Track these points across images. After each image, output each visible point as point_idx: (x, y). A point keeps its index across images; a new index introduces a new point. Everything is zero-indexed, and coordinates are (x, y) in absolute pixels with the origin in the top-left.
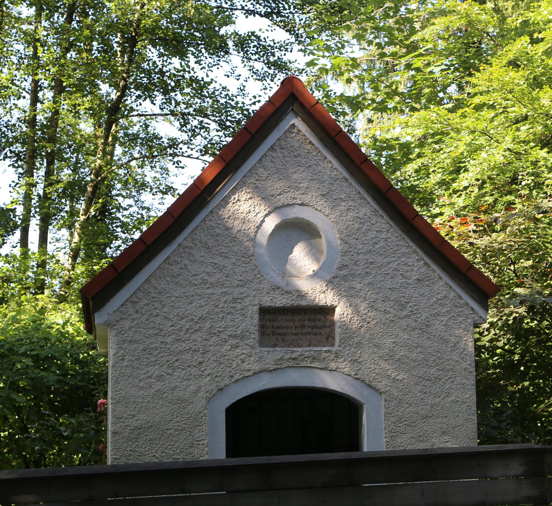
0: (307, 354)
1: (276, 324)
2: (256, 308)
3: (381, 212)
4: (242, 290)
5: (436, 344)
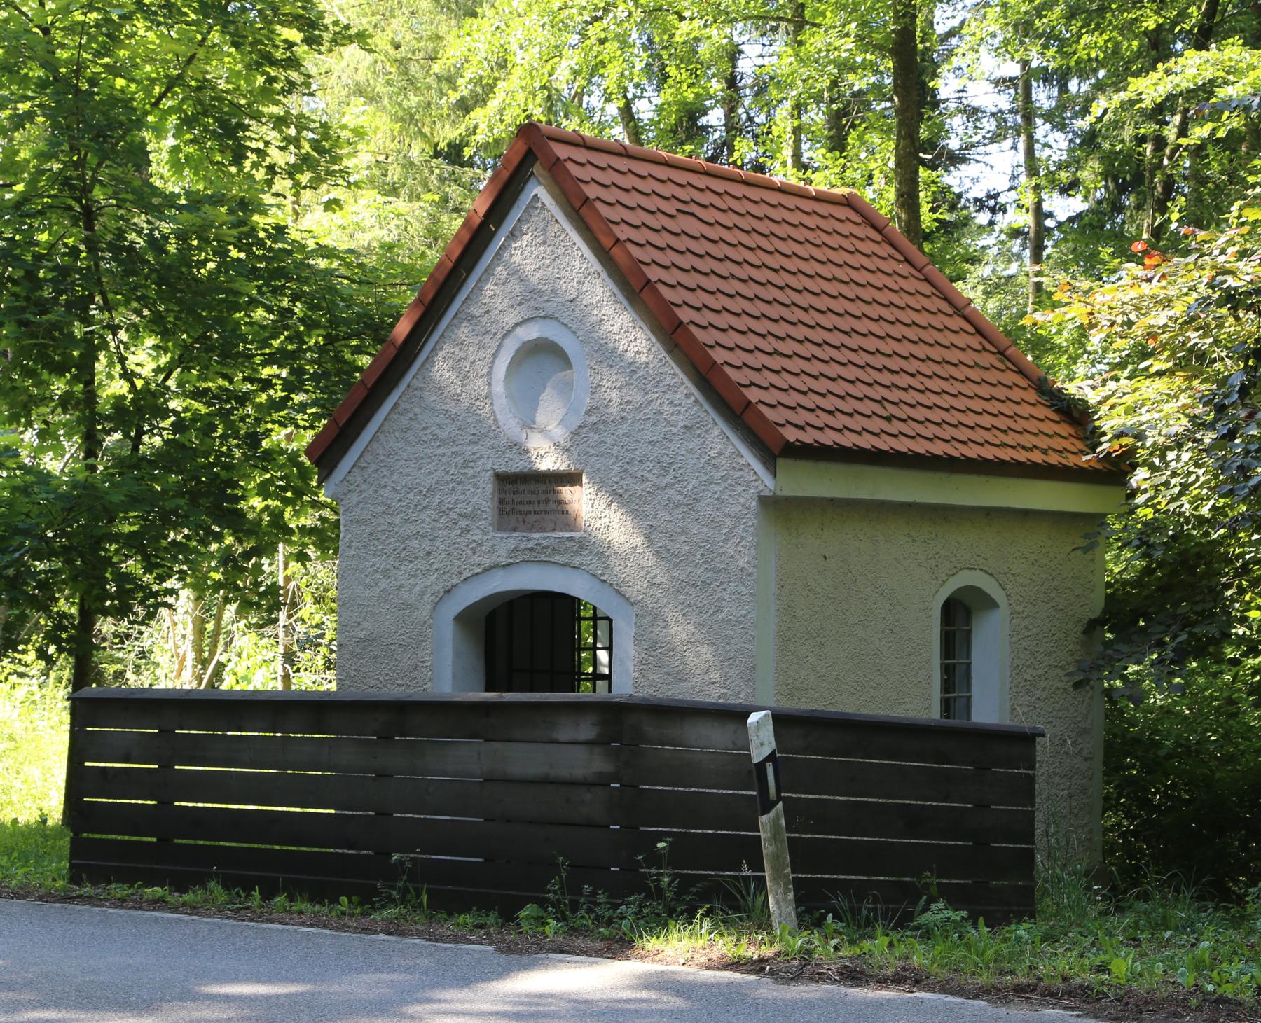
0: (545, 543)
1: (517, 497)
5: (705, 529)
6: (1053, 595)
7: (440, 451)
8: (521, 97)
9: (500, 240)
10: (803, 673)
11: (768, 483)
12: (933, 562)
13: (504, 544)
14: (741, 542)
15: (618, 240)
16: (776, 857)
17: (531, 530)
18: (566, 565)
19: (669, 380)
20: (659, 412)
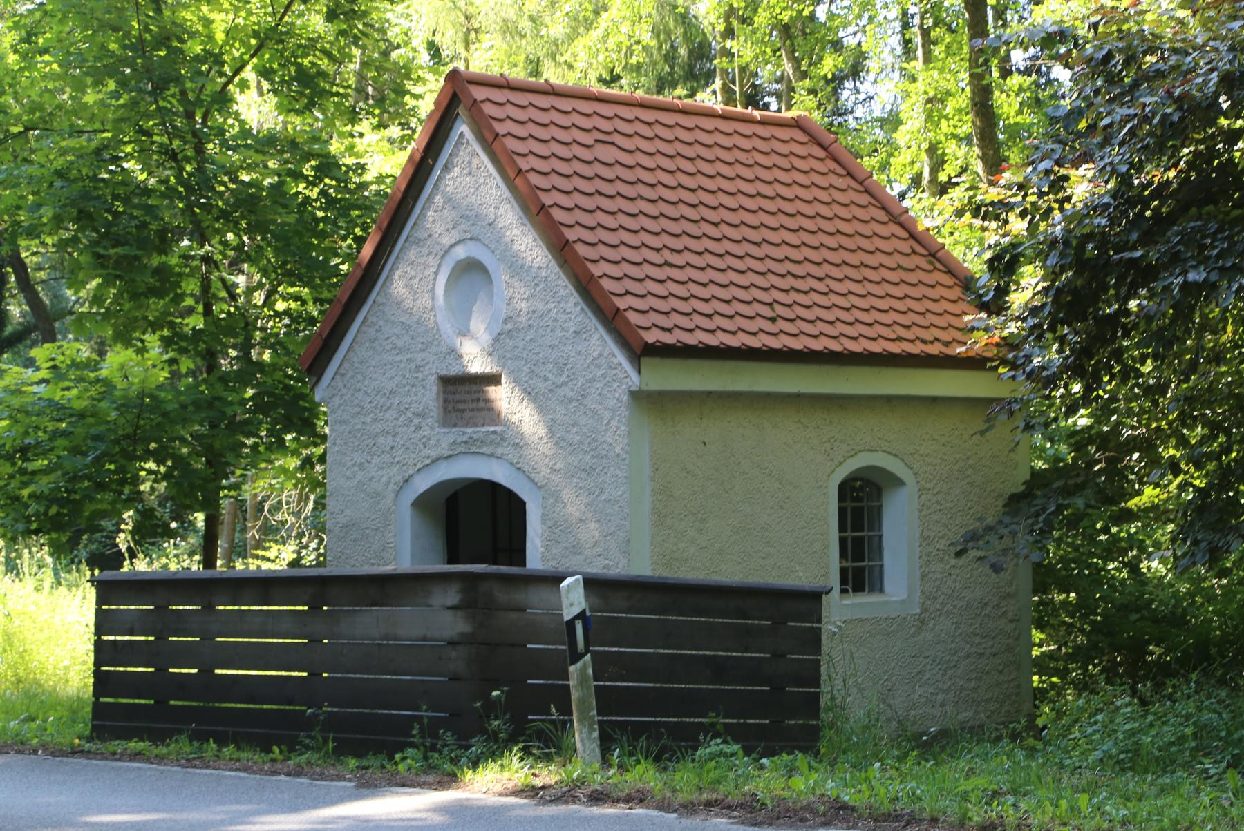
0: (476, 437)
1: (457, 397)
2: (433, 378)
6: (969, 472)
7: (398, 358)
8: (625, 27)
9: (437, 172)
10: (682, 546)
11: (634, 380)
12: (828, 446)
13: (445, 438)
14: (616, 428)
15: (520, 170)
16: (582, 701)
17: (466, 426)
18: (491, 455)
19: (562, 292)
20: (556, 320)
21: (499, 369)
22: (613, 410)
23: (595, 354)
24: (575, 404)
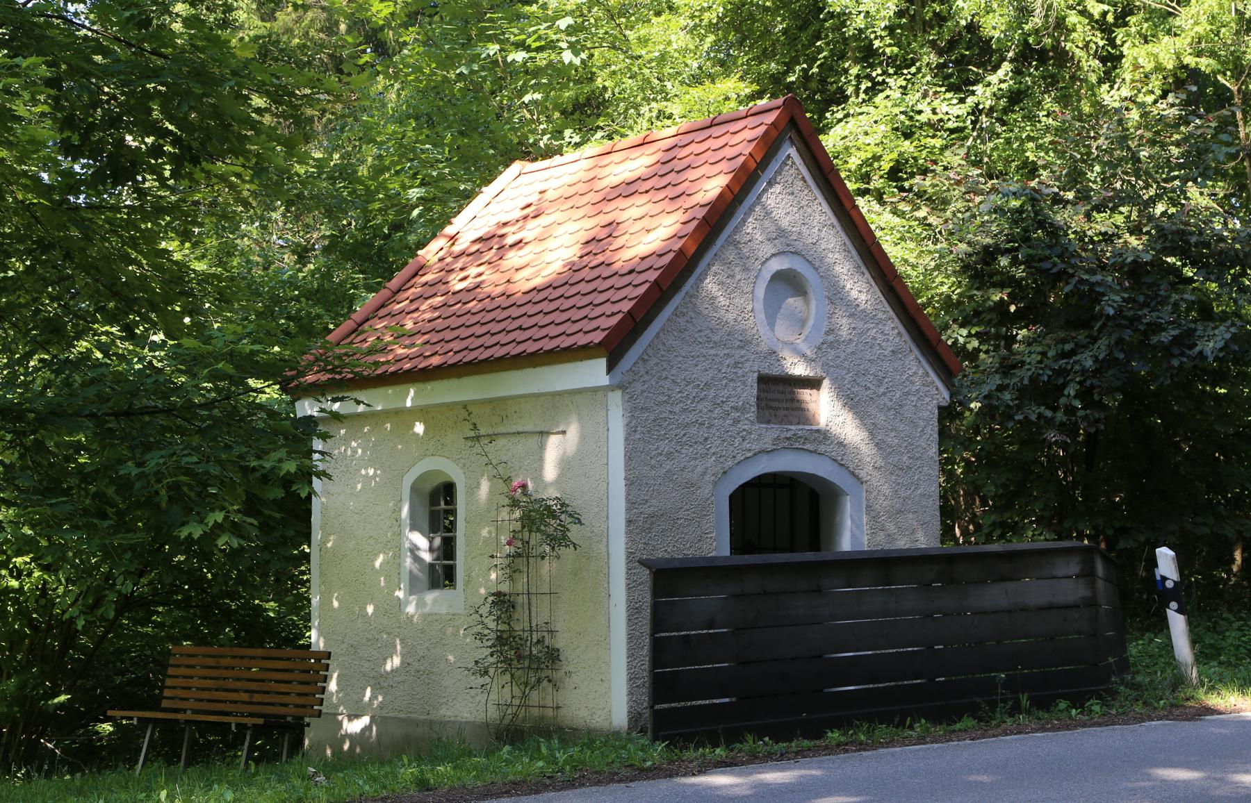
1: (770, 396)
2: (756, 375)
3: (863, 269)
4: (743, 352)
13: (770, 434)
18: (815, 452)
21: (820, 373)
22: (927, 421)
23: (910, 372)
24: (892, 412)
